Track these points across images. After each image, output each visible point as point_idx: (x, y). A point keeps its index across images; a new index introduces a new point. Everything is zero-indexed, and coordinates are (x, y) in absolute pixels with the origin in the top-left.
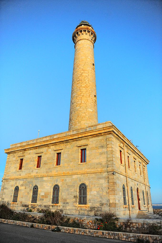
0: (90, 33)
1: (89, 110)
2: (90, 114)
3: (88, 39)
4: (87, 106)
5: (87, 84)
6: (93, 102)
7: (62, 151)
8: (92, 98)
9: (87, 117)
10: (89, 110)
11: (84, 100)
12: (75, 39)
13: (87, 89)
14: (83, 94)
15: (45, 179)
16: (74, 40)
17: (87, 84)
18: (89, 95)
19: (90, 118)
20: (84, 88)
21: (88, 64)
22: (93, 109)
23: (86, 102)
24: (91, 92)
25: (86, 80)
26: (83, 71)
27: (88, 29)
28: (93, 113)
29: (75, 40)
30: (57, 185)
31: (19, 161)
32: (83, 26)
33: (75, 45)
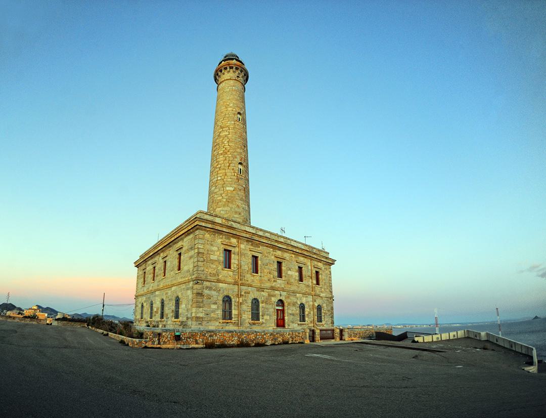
0: (234, 69)
1: (228, 188)
2: (229, 195)
3: (229, 78)
4: (224, 184)
5: (226, 148)
6: (236, 174)
7: (167, 258)
8: (233, 169)
9: (225, 200)
10: (228, 188)
11: (221, 175)
12: (217, 78)
13: (226, 155)
14: (219, 166)
15: (157, 293)
16: (216, 80)
17: (226, 148)
18: (228, 164)
19: (230, 201)
20: (222, 156)
21: (229, 115)
22: (234, 185)
23: (223, 177)
24: (231, 159)
25: (225, 142)
26: (222, 130)
27: (229, 64)
28: (234, 192)
29: (218, 80)
30: (255, 299)
31: (177, 256)
32: (223, 62)
33: (218, 87)
